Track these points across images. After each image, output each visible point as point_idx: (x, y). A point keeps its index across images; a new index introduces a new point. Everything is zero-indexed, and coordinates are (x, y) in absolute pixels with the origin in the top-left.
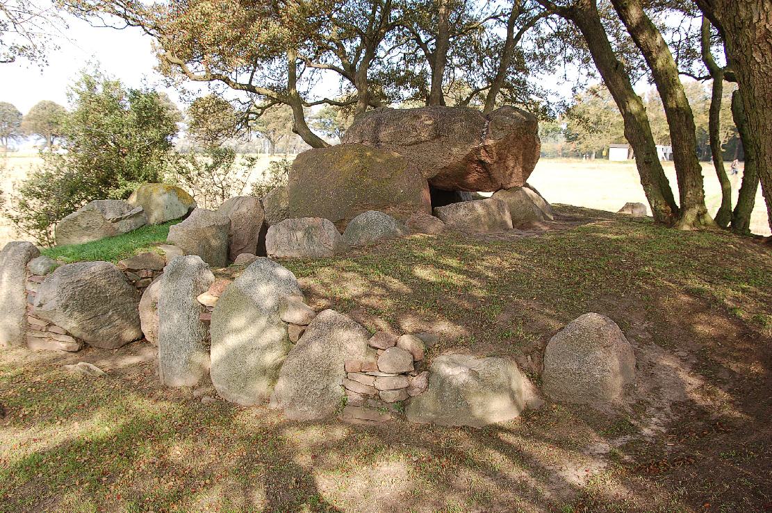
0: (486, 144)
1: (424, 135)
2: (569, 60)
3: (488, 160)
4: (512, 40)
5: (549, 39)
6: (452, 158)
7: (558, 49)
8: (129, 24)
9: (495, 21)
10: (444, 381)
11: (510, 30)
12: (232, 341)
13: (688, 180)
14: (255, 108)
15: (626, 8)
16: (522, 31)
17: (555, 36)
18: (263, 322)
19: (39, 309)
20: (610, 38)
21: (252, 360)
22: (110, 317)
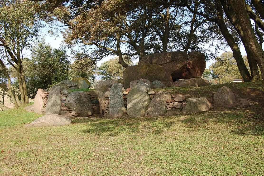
0: (189, 62)
1: (168, 61)
2: (214, 38)
3: (190, 68)
4: (192, 31)
5: (206, 30)
6: (178, 67)
7: (209, 34)
8: (65, 25)
9: (185, 24)
10: (191, 102)
11: (192, 28)
12: (134, 101)
13: (253, 68)
14: (99, 57)
15: (231, 18)
16: (196, 28)
17: (208, 30)
18: (144, 95)
19: (68, 102)
20: (229, 29)
21: (140, 105)
22: (85, 107)
